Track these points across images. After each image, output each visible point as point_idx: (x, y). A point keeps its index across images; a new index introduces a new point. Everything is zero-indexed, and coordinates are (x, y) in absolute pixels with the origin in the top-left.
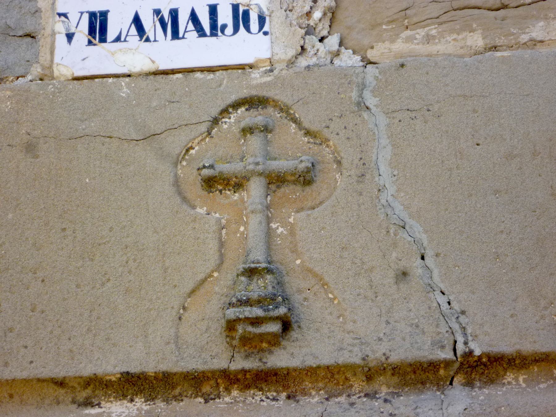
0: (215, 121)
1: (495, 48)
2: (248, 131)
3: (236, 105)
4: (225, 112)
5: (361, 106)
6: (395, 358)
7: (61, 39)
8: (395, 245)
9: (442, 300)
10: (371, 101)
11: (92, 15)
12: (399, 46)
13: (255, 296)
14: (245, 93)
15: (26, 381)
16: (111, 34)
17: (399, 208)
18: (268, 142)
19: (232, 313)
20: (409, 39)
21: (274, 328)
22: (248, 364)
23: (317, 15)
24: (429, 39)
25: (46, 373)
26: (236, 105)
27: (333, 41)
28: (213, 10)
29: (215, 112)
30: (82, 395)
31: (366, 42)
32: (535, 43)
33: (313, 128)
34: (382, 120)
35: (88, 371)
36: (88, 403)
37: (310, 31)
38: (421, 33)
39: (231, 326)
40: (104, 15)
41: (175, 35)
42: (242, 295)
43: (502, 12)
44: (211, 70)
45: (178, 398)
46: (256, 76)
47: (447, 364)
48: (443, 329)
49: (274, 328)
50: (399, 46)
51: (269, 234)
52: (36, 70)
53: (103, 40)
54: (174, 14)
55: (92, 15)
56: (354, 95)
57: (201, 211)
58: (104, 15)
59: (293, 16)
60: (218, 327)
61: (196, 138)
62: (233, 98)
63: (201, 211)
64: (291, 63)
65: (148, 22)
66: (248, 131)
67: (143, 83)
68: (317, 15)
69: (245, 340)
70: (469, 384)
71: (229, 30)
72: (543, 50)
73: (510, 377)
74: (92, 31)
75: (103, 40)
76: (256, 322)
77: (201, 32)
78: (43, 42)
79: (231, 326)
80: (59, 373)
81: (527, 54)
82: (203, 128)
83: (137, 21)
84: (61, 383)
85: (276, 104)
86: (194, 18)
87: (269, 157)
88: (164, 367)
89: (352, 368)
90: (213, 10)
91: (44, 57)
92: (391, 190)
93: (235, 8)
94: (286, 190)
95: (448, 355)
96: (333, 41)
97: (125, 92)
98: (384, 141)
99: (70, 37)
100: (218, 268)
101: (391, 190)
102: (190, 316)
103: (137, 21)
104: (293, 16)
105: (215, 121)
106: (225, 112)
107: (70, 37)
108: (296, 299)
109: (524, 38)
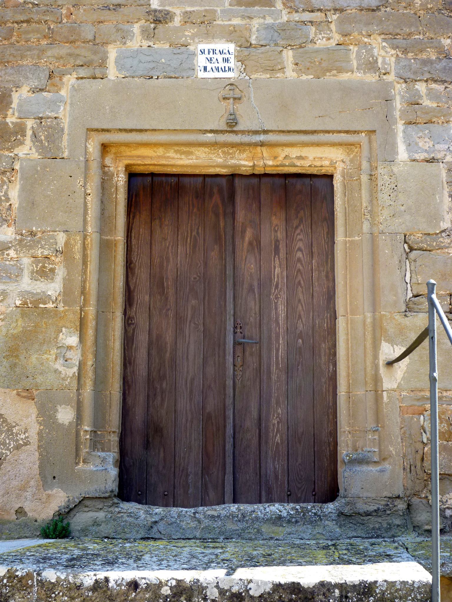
0: (225, 87)
1: (271, 78)
2: (230, 90)
3: (228, 85)
4: (227, 86)
5: (249, 86)
6: (253, 130)
7: (199, 71)
8: (254, 111)
9: (260, 121)
10: (251, 86)
11: (204, 67)
12: (256, 76)
13: (232, 118)
14: (230, 83)
15: (195, 130)
16: (208, 71)
17: (254, 105)
18: (233, 92)
19: (228, 121)
20: (257, 75)
21: (234, 124)
22: (230, 129)
23: (242, 69)
24: (261, 75)
25: (198, 129)
26: (228, 85)
27: (245, 74)
28: (225, 67)
29: (225, 86)
30: (204, 132)
31: (250, 75)
32: (278, 77)
33: (241, 90)
34: (252, 89)
35: (205, 129)
36: (204, 134)
37: (241, 72)
38: (259, 74)
39: (228, 123)
40: (206, 67)
41: (218, 72)
42: (230, 118)
43: (273, 71)
44: (224, 78)
45: (219, 134)
46: (232, 80)
47: (261, 131)
48: (260, 125)
49: (234, 124)
50: (256, 76)
51: (234, 108)
52: (195, 76)
53: (206, 71)
54: (218, 67)
55: (204, 67)
56: (248, 84)
57: (223, 103)
58: (206, 67)
59: (238, 69)
60: (225, 123)
61: (365, 338)
62: (228, 83)
63: (223, 103)
64: (238, 78)
65: (214, 69)
66: (230, 90)
67: (213, 80)
68: (242, 69)
69: (230, 125)
70: (264, 134)
71: (227, 71)
72: (279, 78)
73: (270, 133)
74: (204, 70)
75: (206, 71)
76: (232, 123)
77: (223, 72)
78: (196, 71)
79: (228, 123)
80: (200, 129)
81: (276, 79)
82: (223, 89)
83: (212, 68)
84: (200, 130)
85: (235, 85)
86: (221, 68)
87: (234, 94)
88: (217, 129)
89: (246, 131)
90: (225, 67)
91: (196, 73)
92: (253, 102)
93: (229, 67)
94: (236, 100)
95: (261, 129)
96: (245, 74)
97: (210, 81)
98: (253, 93)
99: (201, 70)
100: (225, 113)
101: (253, 102)
102: (221, 121)
103: (212, 68)
104: (238, 69)
105: (225, 87)
106: (227, 86)
107: (201, 70)
108: (238, 119)
109: (276, 76)
